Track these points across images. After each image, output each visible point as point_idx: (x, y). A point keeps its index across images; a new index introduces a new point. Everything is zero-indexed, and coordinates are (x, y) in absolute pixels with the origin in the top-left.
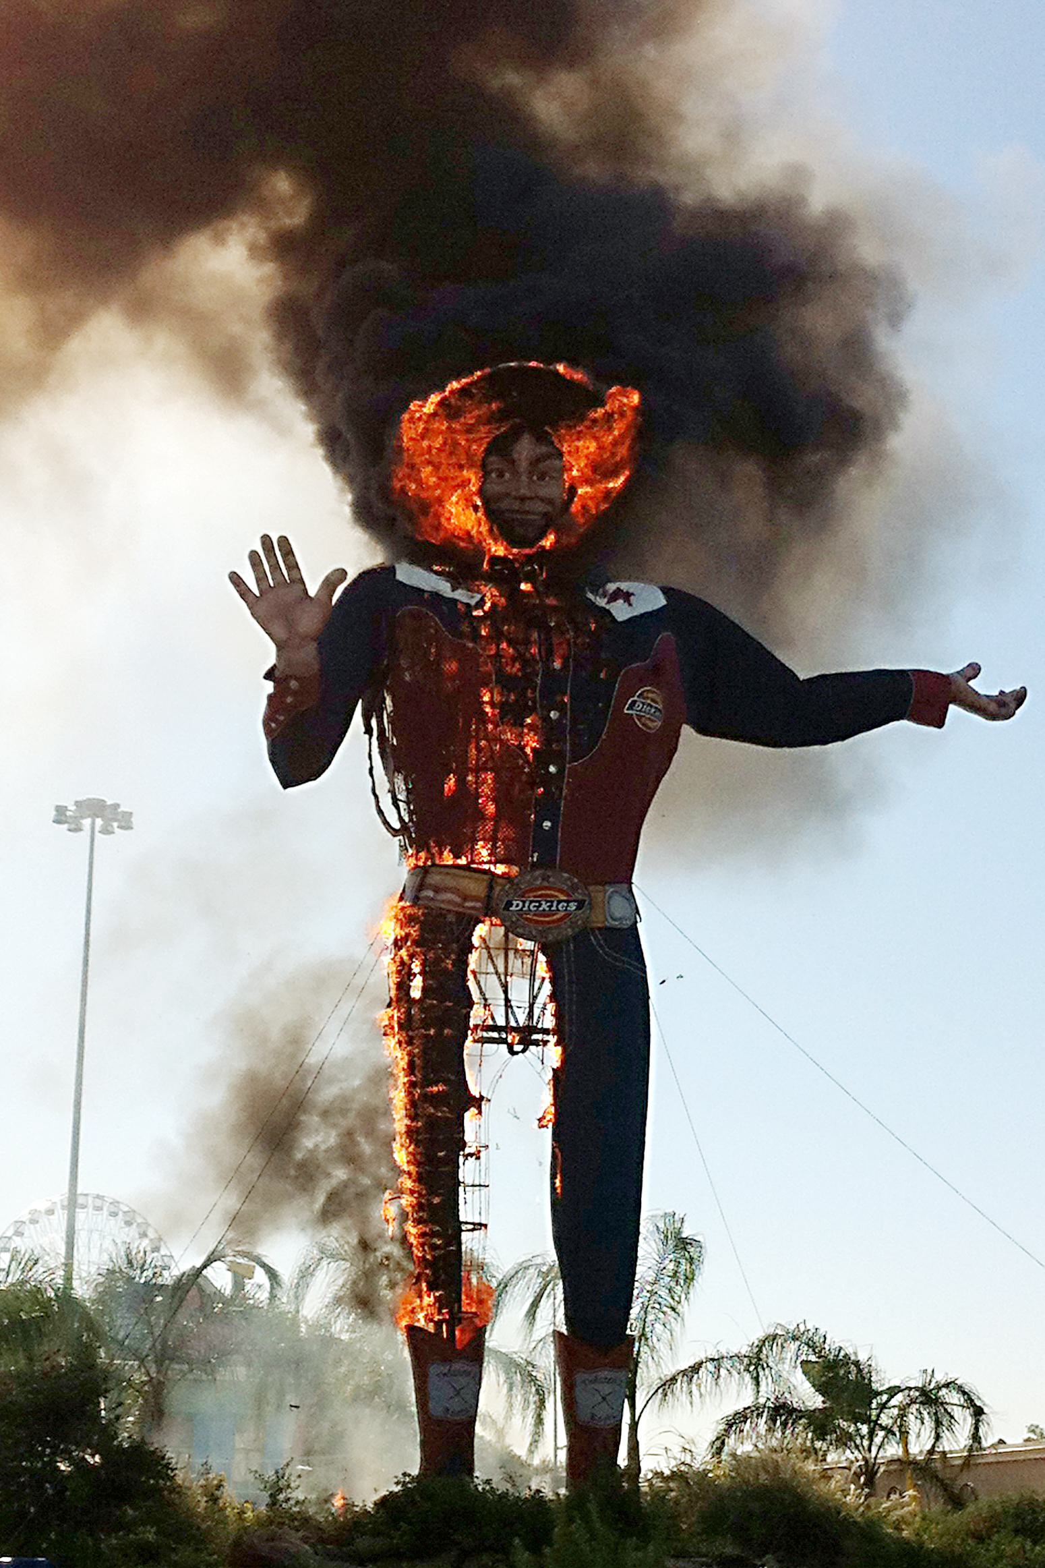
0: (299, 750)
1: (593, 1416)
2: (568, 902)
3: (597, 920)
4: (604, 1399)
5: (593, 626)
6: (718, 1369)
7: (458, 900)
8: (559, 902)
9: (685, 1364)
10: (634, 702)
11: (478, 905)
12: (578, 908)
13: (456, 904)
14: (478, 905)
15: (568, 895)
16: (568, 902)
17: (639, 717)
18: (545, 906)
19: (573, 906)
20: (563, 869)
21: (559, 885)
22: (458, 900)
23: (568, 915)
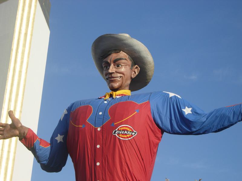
10: (116, 131)
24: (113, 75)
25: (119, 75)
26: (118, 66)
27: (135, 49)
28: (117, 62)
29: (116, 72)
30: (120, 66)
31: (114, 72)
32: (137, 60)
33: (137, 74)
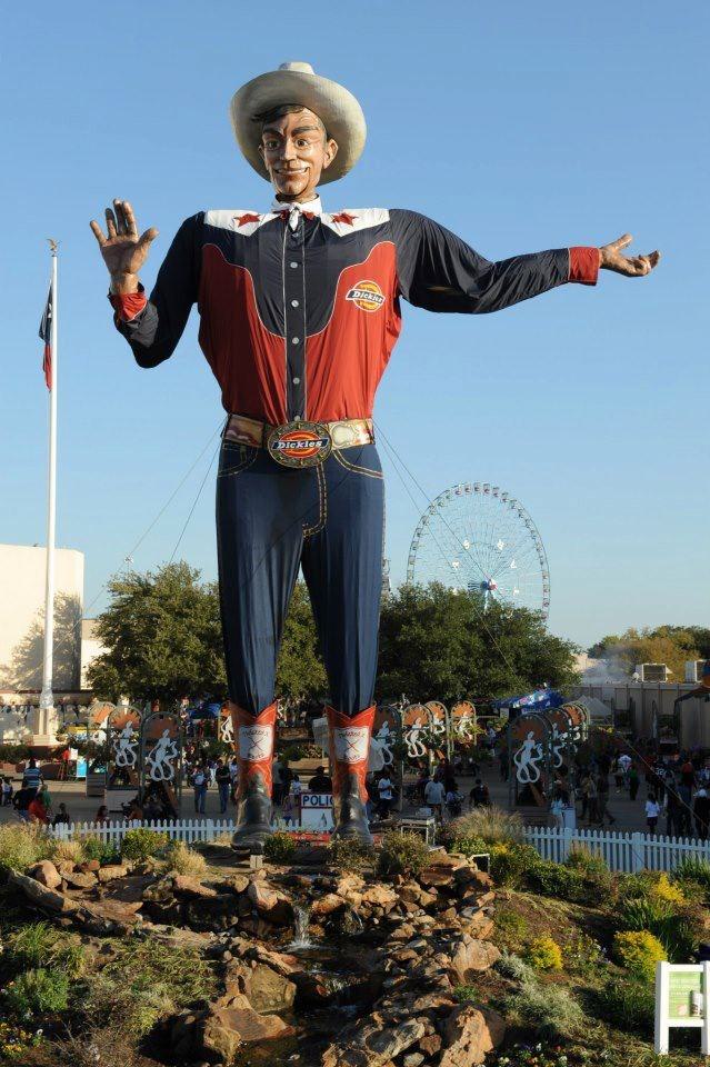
2: (315, 441)
7: (234, 434)
10: (352, 293)
12: (324, 444)
15: (314, 436)
16: (315, 441)
17: (358, 302)
18: (300, 445)
19: (319, 444)
25: (304, 165)
26: (301, 144)
31: (295, 157)
32: (336, 130)
33: (332, 158)
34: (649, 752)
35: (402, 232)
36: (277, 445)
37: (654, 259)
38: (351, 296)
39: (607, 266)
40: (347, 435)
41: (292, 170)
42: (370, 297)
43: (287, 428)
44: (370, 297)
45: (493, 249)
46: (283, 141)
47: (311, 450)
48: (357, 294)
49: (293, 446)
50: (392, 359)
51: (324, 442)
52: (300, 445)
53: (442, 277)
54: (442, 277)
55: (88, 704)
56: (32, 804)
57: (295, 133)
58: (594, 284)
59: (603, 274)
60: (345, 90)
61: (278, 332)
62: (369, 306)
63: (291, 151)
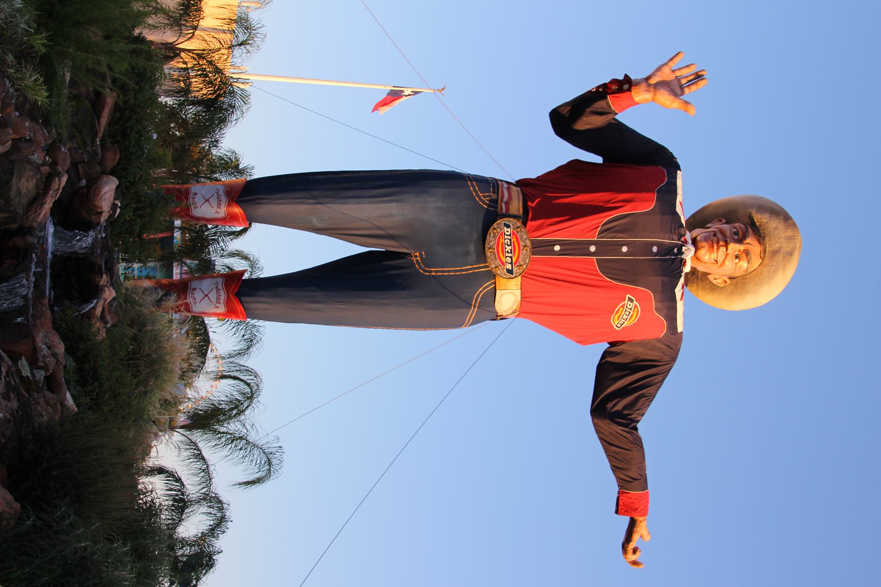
0: (564, 121)
1: (195, 289)
2: (511, 263)
3: (501, 282)
4: (206, 296)
5: (155, 136)
6: (203, 471)
7: (505, 199)
8: (511, 258)
9: (205, 453)
10: (631, 301)
11: (504, 211)
12: (508, 271)
13: (502, 200)
14: (504, 211)
15: (516, 263)
16: (511, 263)
17: (623, 306)
18: (508, 248)
19: (509, 267)
20: (532, 260)
21: (521, 257)
22: (505, 199)
23: (503, 264)
24: (723, 249)
26: (737, 257)
27: (775, 272)
28: (744, 255)
29: (727, 255)
30: (737, 261)
31: (729, 251)
33: (714, 282)
34: (20, 519)
35: (669, 344)
36: (508, 226)
37: (635, 563)
38: (630, 299)
39: (633, 524)
40: (508, 297)
41: (718, 249)
42: (625, 317)
43: (525, 237)
44: (625, 317)
45: (651, 425)
46: (740, 241)
47: (504, 260)
48: (631, 305)
49: (508, 241)
50: (791, 213)
51: (510, 272)
52: (508, 248)
53: (622, 389)
54: (622, 389)
55: (206, 284)
56: (152, 36)
57: (747, 253)
58: (617, 512)
59: (625, 520)
60: (778, 292)
61: (601, 232)
62: (617, 316)
63: (734, 247)
